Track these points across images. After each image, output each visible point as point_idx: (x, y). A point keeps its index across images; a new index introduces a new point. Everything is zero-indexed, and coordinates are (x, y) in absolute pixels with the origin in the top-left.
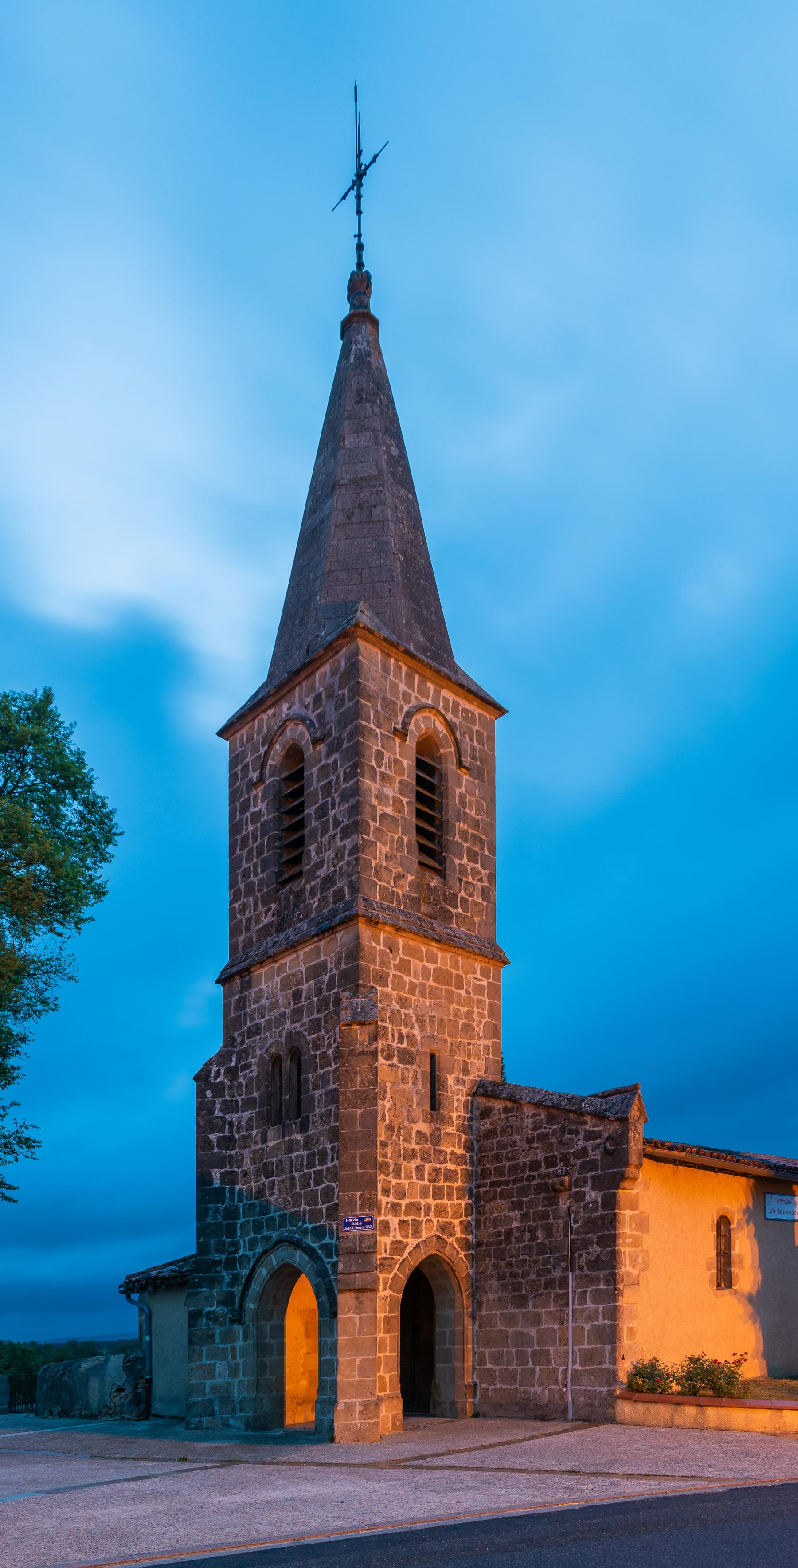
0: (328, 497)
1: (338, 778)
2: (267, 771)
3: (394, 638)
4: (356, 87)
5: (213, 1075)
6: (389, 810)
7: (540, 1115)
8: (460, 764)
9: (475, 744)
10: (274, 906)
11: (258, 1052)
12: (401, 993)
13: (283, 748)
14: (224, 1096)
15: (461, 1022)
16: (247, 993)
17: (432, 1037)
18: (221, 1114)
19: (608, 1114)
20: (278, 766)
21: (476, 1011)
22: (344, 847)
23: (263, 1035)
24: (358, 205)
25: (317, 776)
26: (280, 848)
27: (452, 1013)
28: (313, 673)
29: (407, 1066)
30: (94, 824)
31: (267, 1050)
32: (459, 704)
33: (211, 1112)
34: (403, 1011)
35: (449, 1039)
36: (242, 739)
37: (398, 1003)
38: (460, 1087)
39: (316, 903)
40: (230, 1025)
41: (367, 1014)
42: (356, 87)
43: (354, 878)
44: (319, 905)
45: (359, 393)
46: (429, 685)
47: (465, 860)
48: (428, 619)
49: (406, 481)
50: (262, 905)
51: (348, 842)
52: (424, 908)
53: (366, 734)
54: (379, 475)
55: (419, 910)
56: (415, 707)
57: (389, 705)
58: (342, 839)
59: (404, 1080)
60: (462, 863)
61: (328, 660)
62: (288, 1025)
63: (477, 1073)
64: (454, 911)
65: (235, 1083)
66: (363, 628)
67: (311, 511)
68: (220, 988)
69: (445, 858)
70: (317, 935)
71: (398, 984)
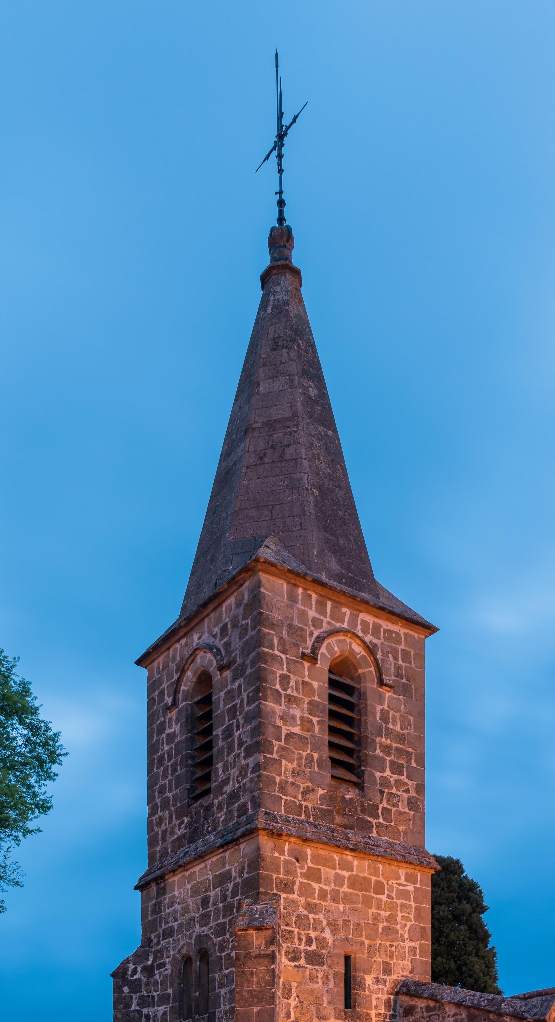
0: (241, 440)
1: (242, 701)
2: (180, 695)
3: (302, 569)
4: (277, 55)
5: (130, 972)
6: (296, 730)
7: (461, 1014)
8: (381, 683)
9: (400, 662)
10: (186, 819)
11: (172, 953)
12: (309, 899)
13: (194, 674)
14: (141, 992)
15: (381, 926)
16: (162, 899)
17: (346, 940)
18: (137, 1008)
19: (526, 1015)
20: (191, 691)
21: (400, 914)
22: (247, 765)
23: (176, 937)
24: (280, 165)
25: (224, 700)
26: (192, 766)
27: (370, 916)
28: (220, 605)
29: (317, 967)
30: (39, 746)
31: (179, 951)
32: (380, 626)
33: (128, 1006)
34: (311, 916)
35: (367, 942)
36: (158, 667)
37: (306, 909)
38: (380, 986)
39: (223, 817)
40: (149, 927)
41: (264, 919)
42: (277, 55)
43: (256, 794)
44: (225, 819)
45: (275, 341)
46: (344, 610)
47: (388, 773)
48: (345, 548)
49: (326, 419)
50: (176, 818)
51: (251, 761)
52: (337, 819)
53: (269, 660)
54: (293, 417)
55: (332, 822)
56: (327, 632)
57: (297, 633)
58: (245, 758)
59: (313, 979)
60: (385, 775)
61: (233, 593)
62: (198, 929)
63: (401, 973)
64: (374, 821)
65: (152, 980)
66: (265, 562)
67: (226, 454)
68: (138, 893)
69: (363, 771)
70: (222, 846)
71: (306, 891)
